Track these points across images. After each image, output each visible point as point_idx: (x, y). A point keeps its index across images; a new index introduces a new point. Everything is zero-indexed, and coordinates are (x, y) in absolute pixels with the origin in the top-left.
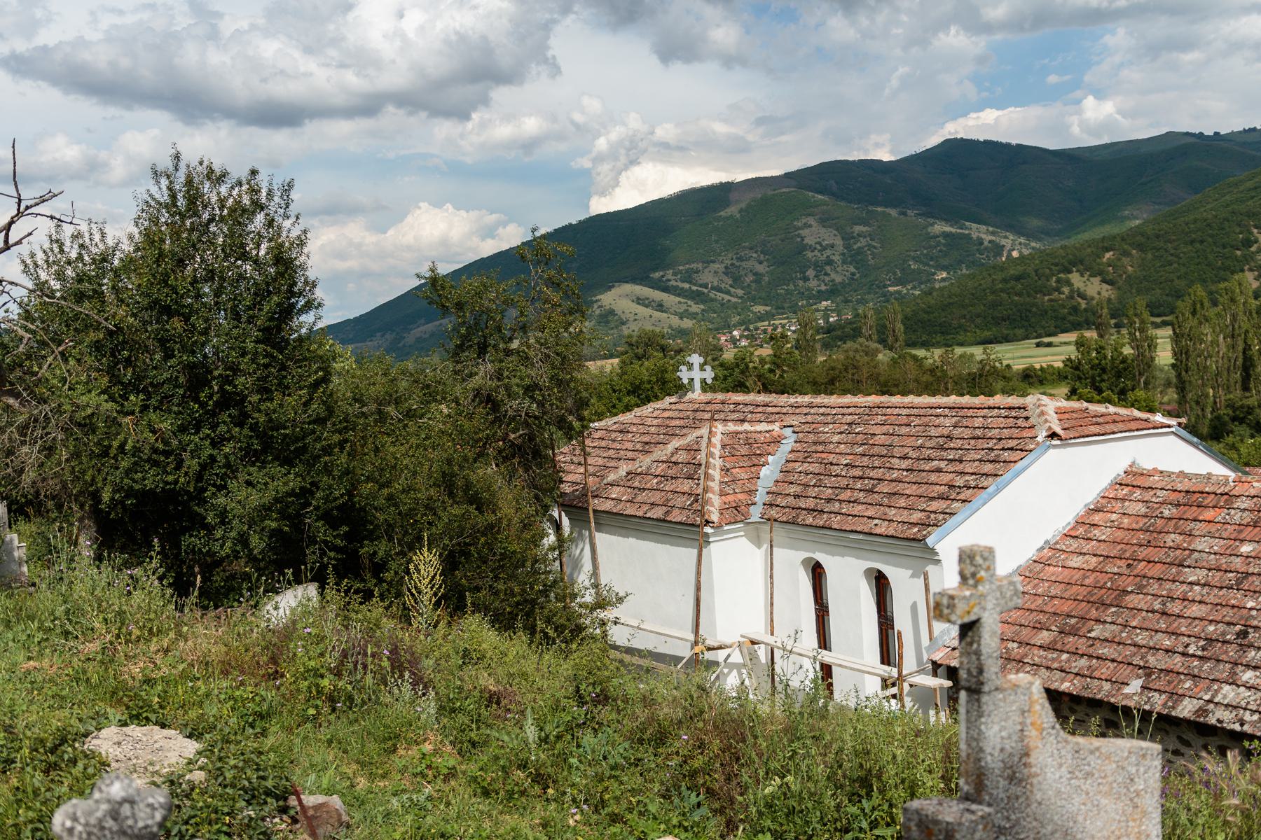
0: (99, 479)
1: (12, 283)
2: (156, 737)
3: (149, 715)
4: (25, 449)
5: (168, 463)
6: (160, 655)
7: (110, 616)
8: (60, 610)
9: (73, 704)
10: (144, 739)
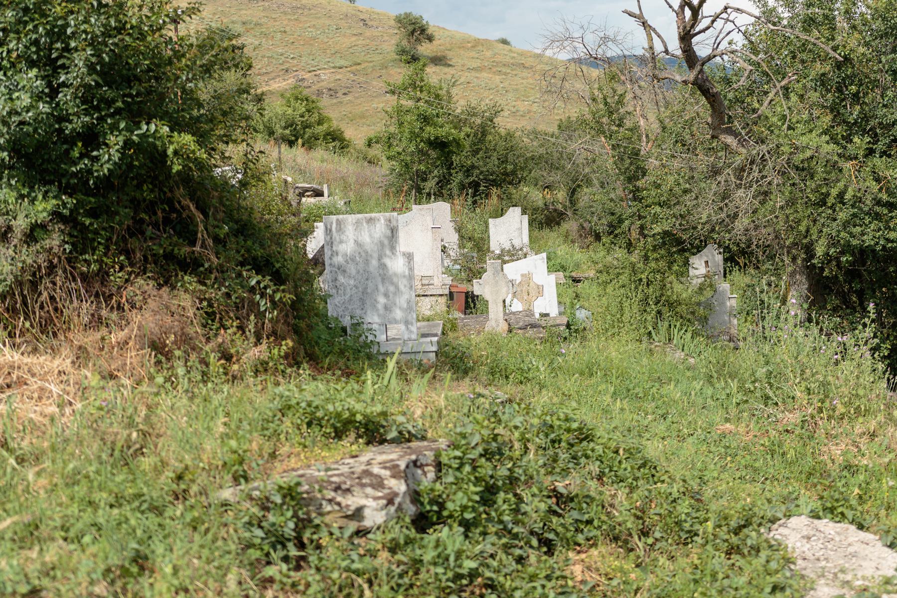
0: (814, 231)
1: (738, 10)
2: (851, 540)
3: (846, 511)
4: (740, 193)
5: (892, 218)
6: (865, 440)
7: (813, 385)
8: (761, 372)
9: (766, 479)
10: (837, 539)
